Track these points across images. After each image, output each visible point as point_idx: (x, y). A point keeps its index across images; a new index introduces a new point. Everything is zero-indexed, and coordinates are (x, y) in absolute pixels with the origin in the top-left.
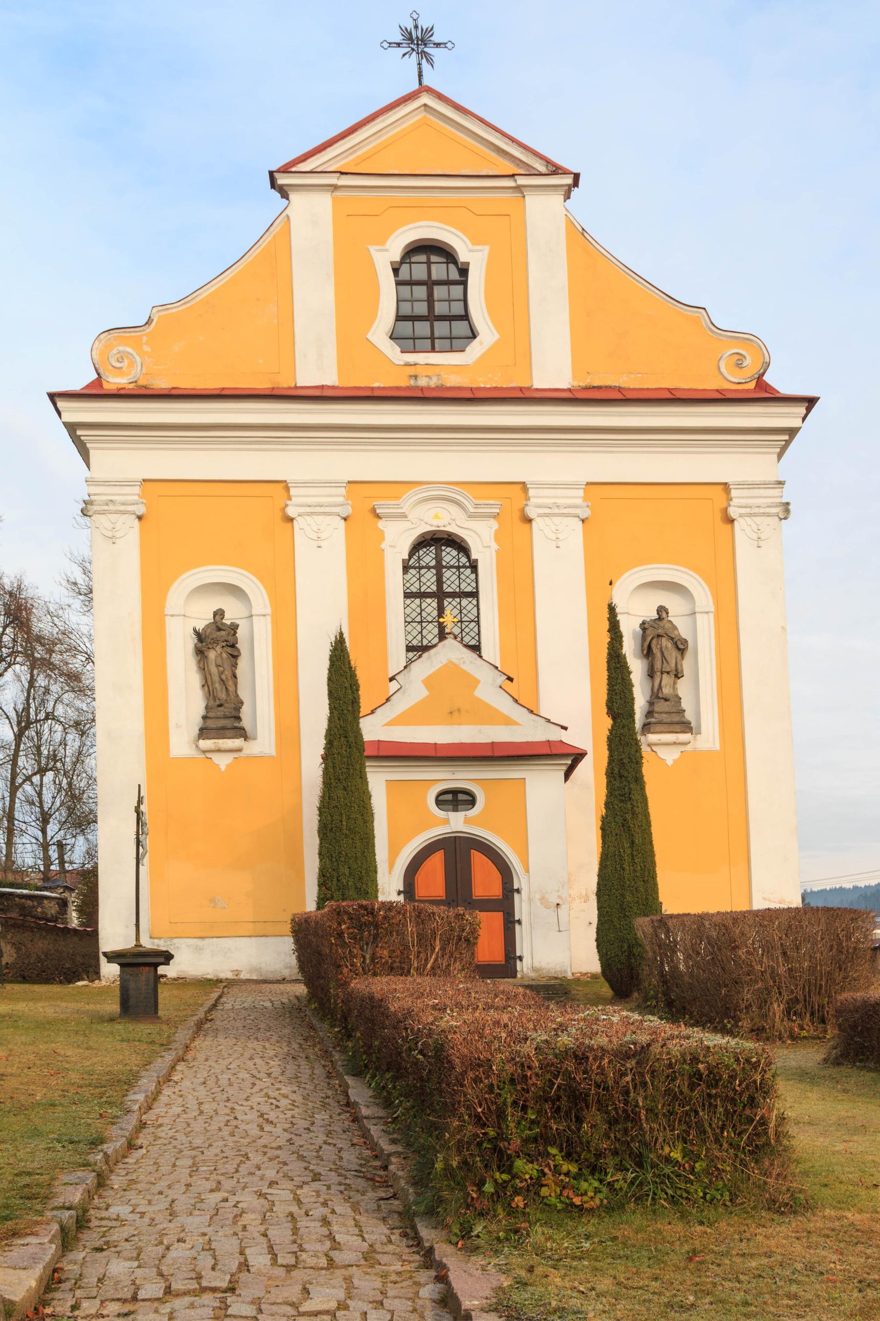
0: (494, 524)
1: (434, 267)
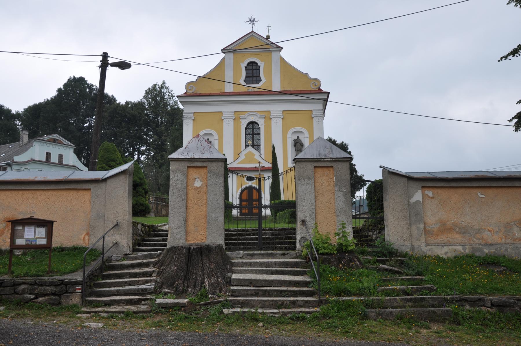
0: (264, 120)
1: (254, 66)
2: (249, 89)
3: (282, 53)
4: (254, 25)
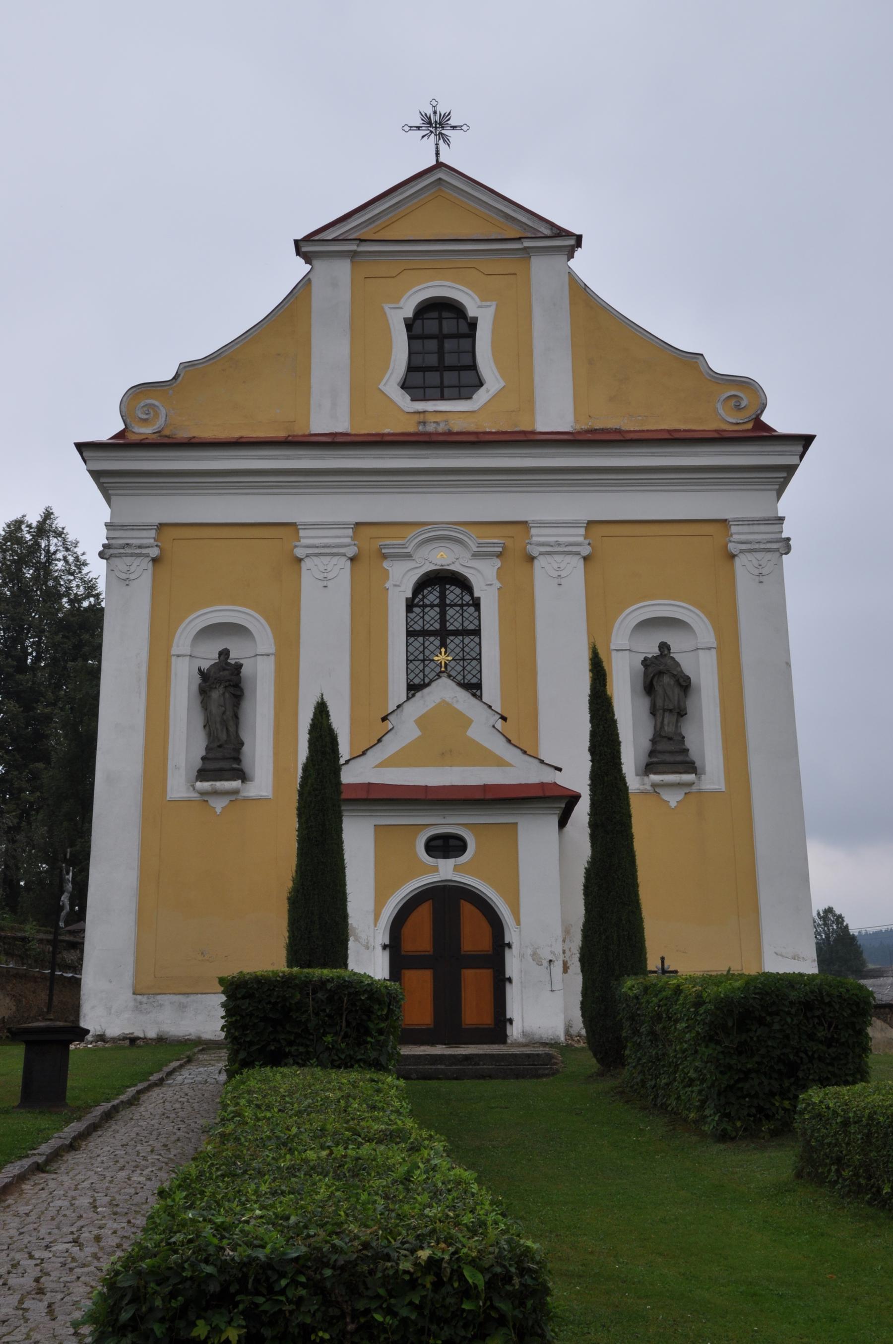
0: (498, 563)
1: (445, 322)
2: (424, 423)
3: (580, 264)
4: (447, 142)
